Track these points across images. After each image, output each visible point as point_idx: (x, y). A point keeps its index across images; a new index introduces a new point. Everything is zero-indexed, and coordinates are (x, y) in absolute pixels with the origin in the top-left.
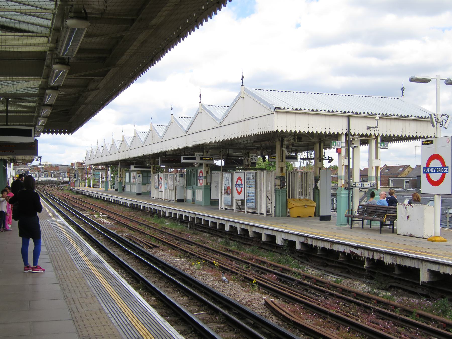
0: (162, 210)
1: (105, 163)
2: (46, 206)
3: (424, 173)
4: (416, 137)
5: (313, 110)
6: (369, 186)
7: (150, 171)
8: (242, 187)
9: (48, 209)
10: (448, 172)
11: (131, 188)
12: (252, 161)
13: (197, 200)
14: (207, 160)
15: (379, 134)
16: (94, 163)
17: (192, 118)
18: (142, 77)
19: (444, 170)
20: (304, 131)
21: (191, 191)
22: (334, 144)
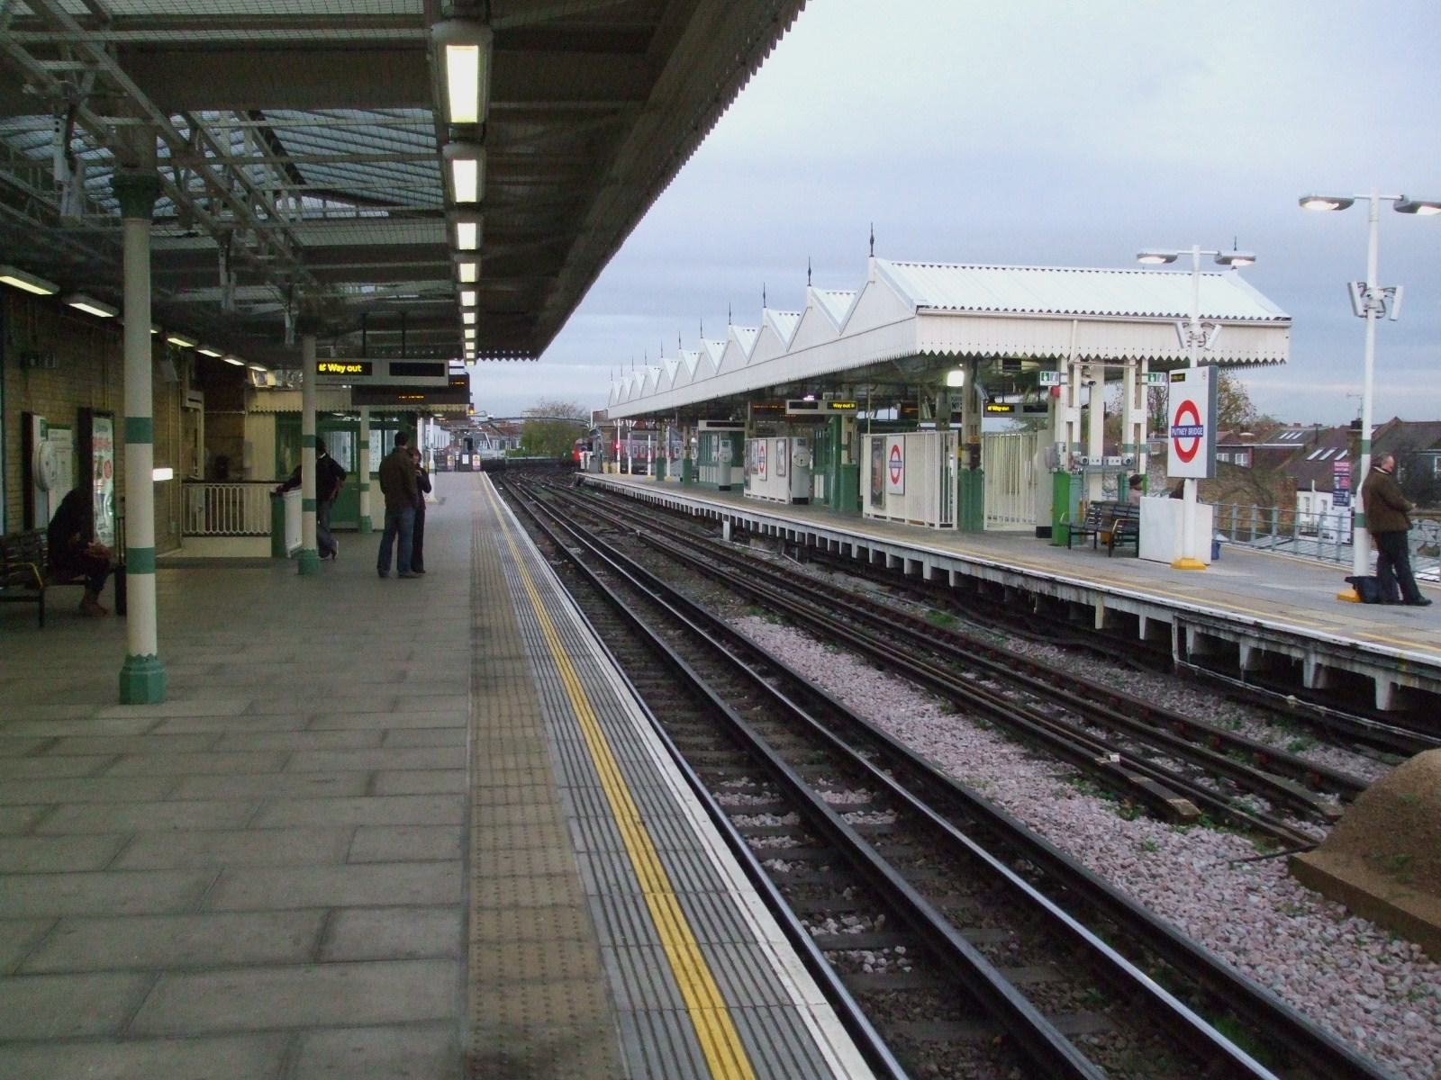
0: (787, 527)
1: (655, 412)
4: (1230, 360)
5: (988, 309)
6: (1119, 464)
7: (742, 434)
9: (506, 522)
11: (713, 475)
12: (954, 410)
15: (1142, 357)
16: (632, 413)
17: (852, 296)
18: (578, 309)
20: (988, 353)
21: (822, 477)
22: (1045, 378)
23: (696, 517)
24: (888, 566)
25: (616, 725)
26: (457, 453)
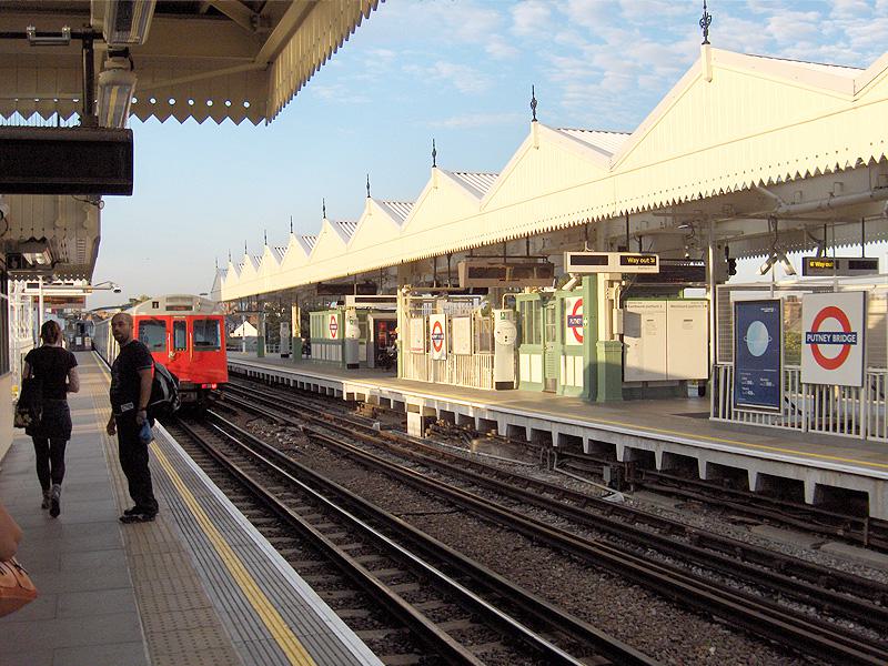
2: (176, 462)
3: (807, 342)
8: (847, 345)
10: (855, 343)
13: (563, 383)
14: (640, 264)
19: (847, 338)
21: (537, 359)
23: (295, 388)
24: (752, 488)
25: (267, 584)
26: (71, 336)
